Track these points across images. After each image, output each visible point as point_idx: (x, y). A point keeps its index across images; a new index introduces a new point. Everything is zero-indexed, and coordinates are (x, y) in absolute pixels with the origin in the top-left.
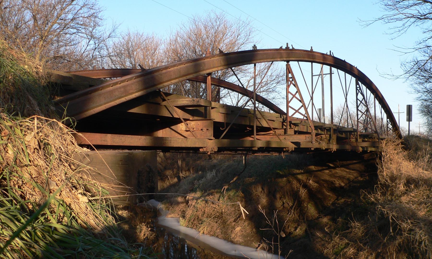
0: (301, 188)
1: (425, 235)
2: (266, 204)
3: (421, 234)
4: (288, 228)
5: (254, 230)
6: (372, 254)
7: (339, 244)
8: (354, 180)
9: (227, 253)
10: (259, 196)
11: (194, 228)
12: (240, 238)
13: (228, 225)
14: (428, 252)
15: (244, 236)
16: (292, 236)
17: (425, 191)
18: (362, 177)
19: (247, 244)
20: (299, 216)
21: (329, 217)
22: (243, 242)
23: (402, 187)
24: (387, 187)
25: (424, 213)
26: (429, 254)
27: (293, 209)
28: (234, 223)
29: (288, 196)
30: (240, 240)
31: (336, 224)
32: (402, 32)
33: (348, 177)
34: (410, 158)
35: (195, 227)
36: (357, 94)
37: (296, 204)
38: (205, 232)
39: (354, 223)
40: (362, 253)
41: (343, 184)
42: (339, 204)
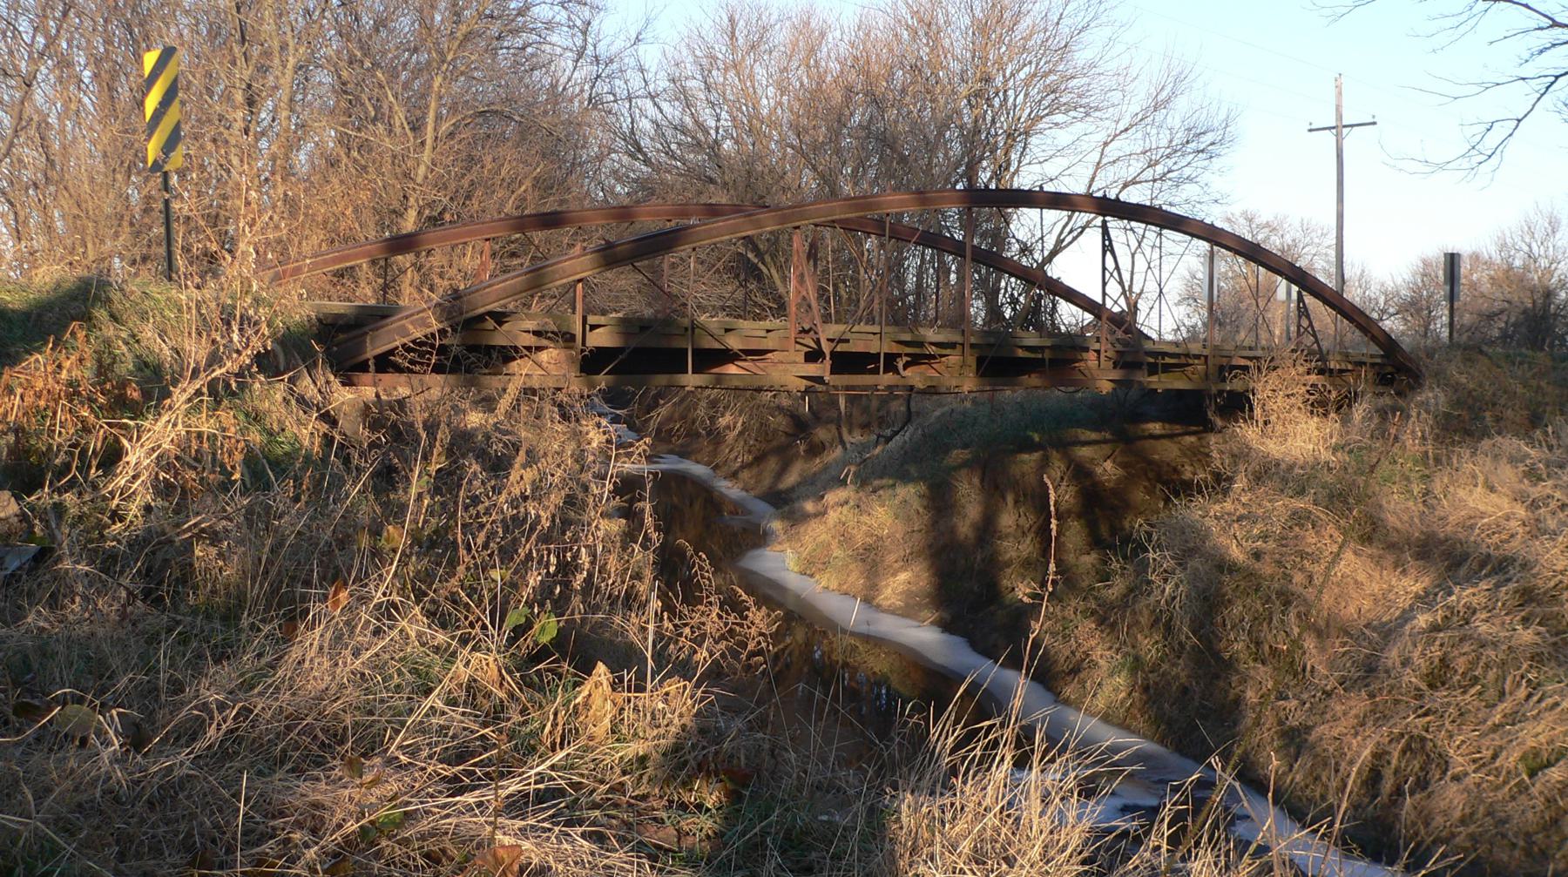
32: (1462, 29)
36: (1300, 317)
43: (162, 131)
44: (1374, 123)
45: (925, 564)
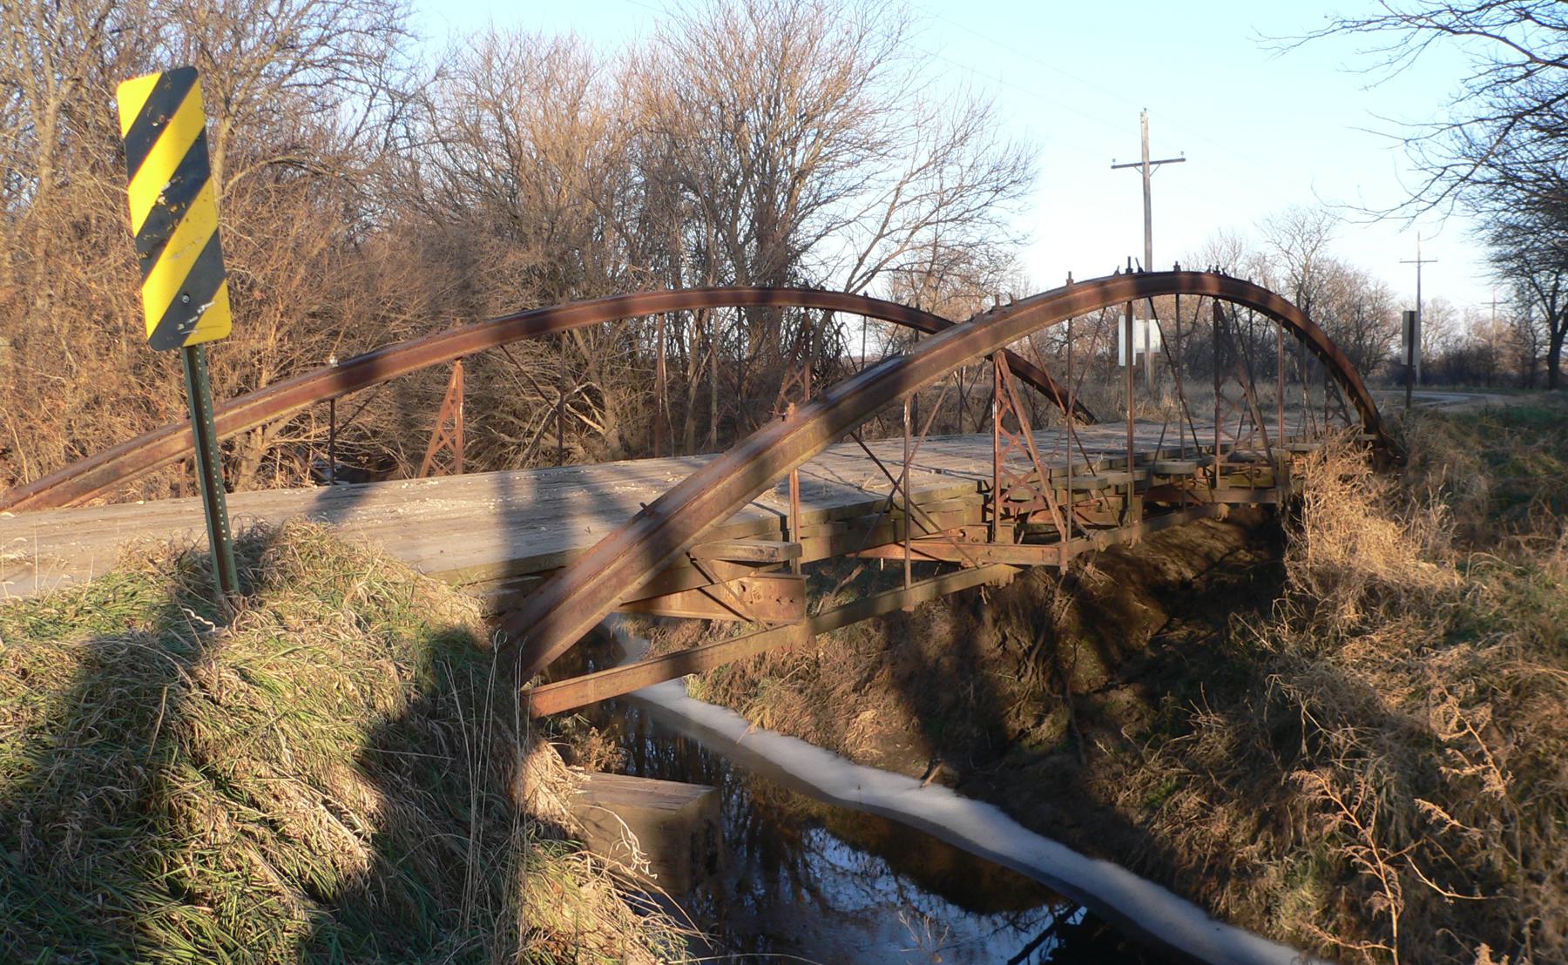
0: (1058, 591)
1: (1392, 770)
2: (949, 639)
3: (1380, 766)
4: (1018, 715)
5: (915, 720)
6: (1248, 813)
7: (1161, 776)
8: (1227, 558)
9: (835, 795)
10: (929, 612)
11: (732, 705)
12: (873, 744)
13: (838, 702)
14: (1394, 818)
15: (884, 739)
16: (1026, 743)
17: (1412, 630)
18: (1249, 551)
19: (891, 765)
20: (1050, 681)
21: (1138, 687)
22: (880, 760)
23: (1353, 610)
24: (1311, 604)
25: (1400, 700)
26: (1396, 824)
27: (1033, 656)
28: (853, 698)
29: (1018, 618)
30: (874, 751)
31: (1158, 710)
32: (1397, 65)
33: (1206, 549)
34: (1397, 506)
35: (735, 704)
37: (1041, 641)
38: (767, 721)
39: (1207, 714)
40: (1221, 809)
41: (1189, 574)
42: (1170, 643)
43: (175, 255)
44: (1183, 160)
45: (891, 699)
